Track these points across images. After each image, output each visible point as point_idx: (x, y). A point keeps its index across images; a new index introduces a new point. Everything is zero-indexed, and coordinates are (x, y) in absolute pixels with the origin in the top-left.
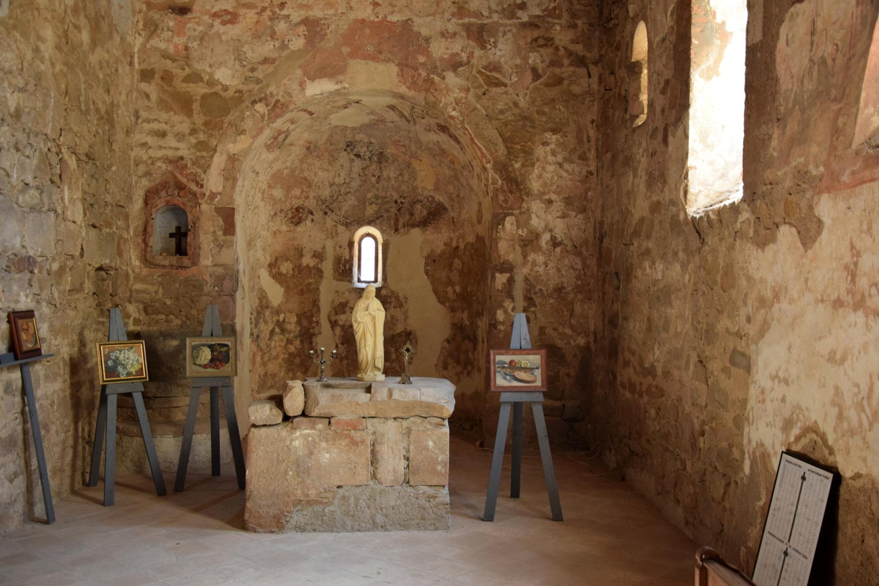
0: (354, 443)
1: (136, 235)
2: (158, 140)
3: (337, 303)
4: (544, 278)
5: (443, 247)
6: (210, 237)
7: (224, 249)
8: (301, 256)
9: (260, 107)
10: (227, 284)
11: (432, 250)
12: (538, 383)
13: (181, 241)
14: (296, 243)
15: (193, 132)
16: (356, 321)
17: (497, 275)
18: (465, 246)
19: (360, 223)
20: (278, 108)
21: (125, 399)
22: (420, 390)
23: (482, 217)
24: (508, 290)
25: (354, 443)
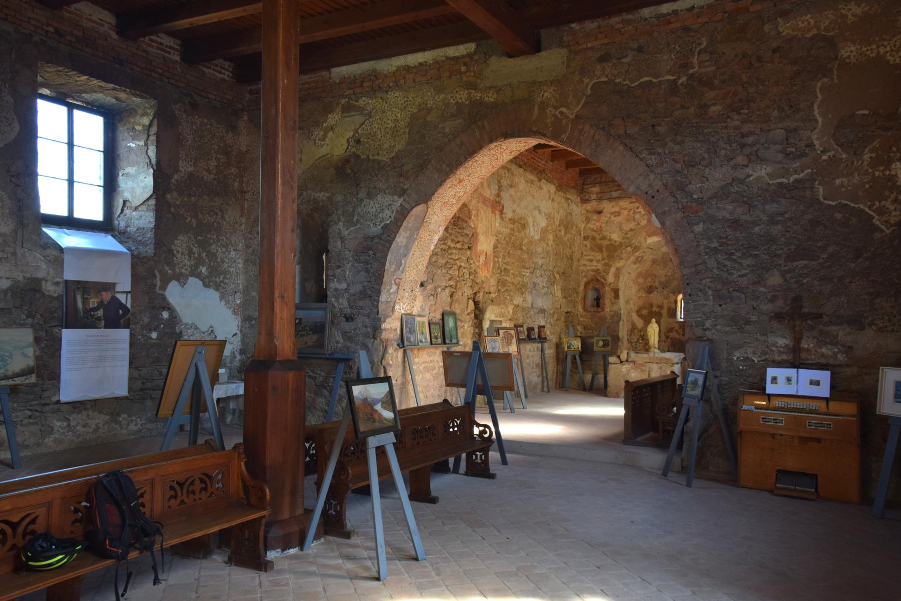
0: (643, 371)
2: (591, 263)
8: (652, 307)
9: (629, 249)
10: (616, 319)
13: (598, 302)
15: (603, 259)
20: (636, 249)
21: (574, 358)
25: (643, 371)
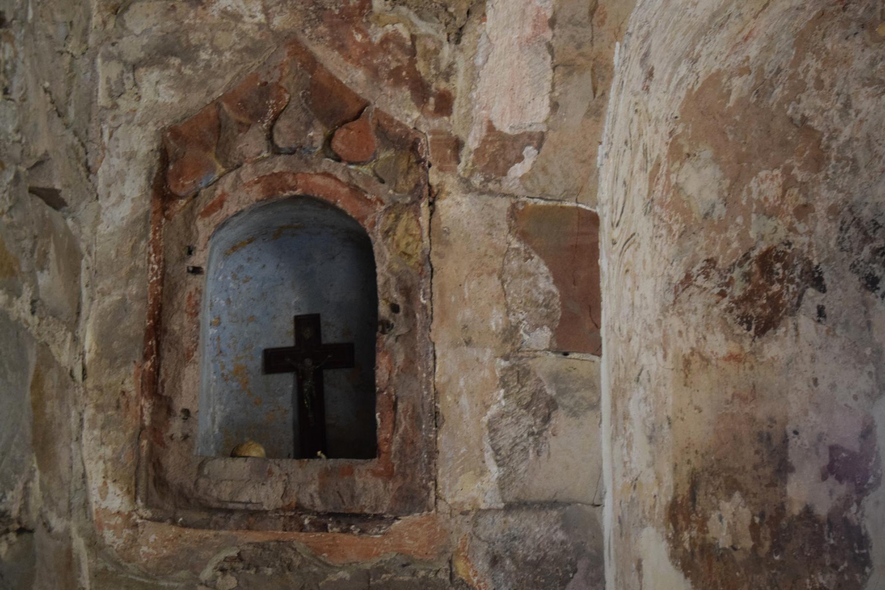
1: (108, 354)
6: (490, 362)
7: (560, 419)
8: (783, 469)
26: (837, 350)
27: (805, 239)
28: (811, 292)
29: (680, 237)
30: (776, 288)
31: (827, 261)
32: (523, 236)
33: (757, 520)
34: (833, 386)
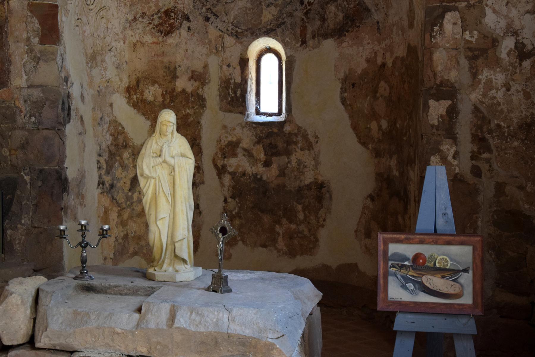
3: (224, 142)
4: (505, 108)
5: (365, 65)
7: (41, 63)
8: (175, 77)
11: (350, 70)
12: (467, 299)
14: (166, 60)
16: (142, 175)
17: (432, 103)
18: (394, 63)
19: (256, 33)
22: (229, 311)
23: (414, 18)
24: (448, 127)
26: (195, 41)
27: (182, 6)
28: (185, 22)
29: (130, 6)
30: (172, 21)
31: (190, 12)
32: (31, 11)
33: (164, 93)
34: (193, 52)
